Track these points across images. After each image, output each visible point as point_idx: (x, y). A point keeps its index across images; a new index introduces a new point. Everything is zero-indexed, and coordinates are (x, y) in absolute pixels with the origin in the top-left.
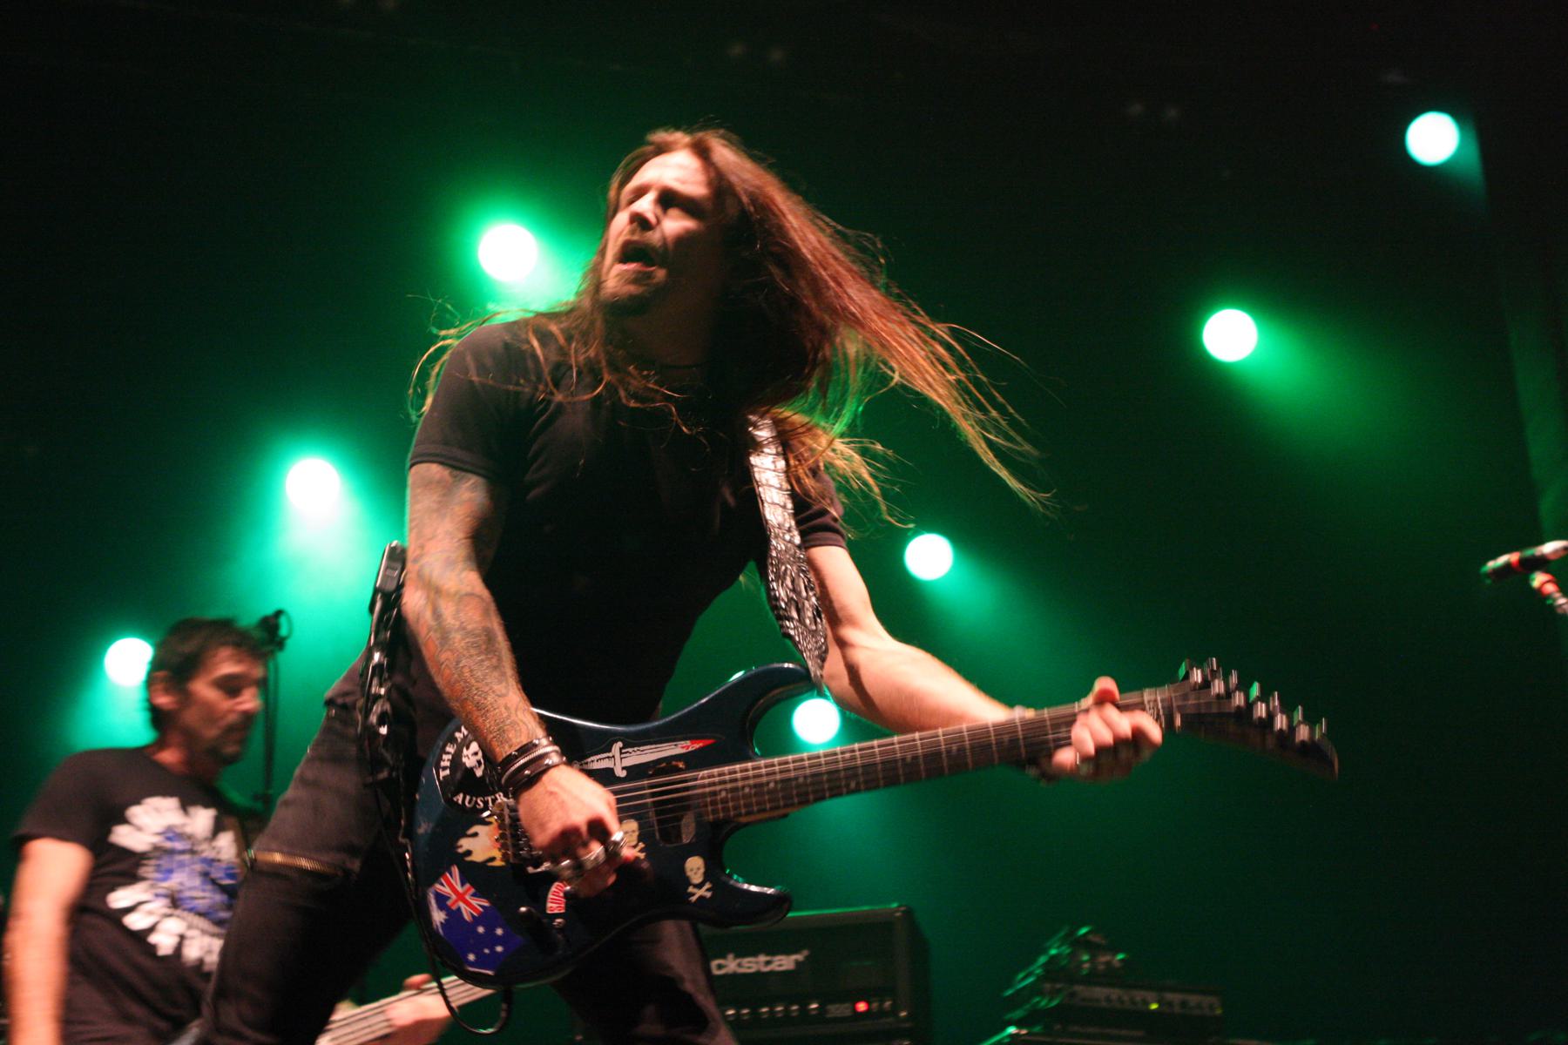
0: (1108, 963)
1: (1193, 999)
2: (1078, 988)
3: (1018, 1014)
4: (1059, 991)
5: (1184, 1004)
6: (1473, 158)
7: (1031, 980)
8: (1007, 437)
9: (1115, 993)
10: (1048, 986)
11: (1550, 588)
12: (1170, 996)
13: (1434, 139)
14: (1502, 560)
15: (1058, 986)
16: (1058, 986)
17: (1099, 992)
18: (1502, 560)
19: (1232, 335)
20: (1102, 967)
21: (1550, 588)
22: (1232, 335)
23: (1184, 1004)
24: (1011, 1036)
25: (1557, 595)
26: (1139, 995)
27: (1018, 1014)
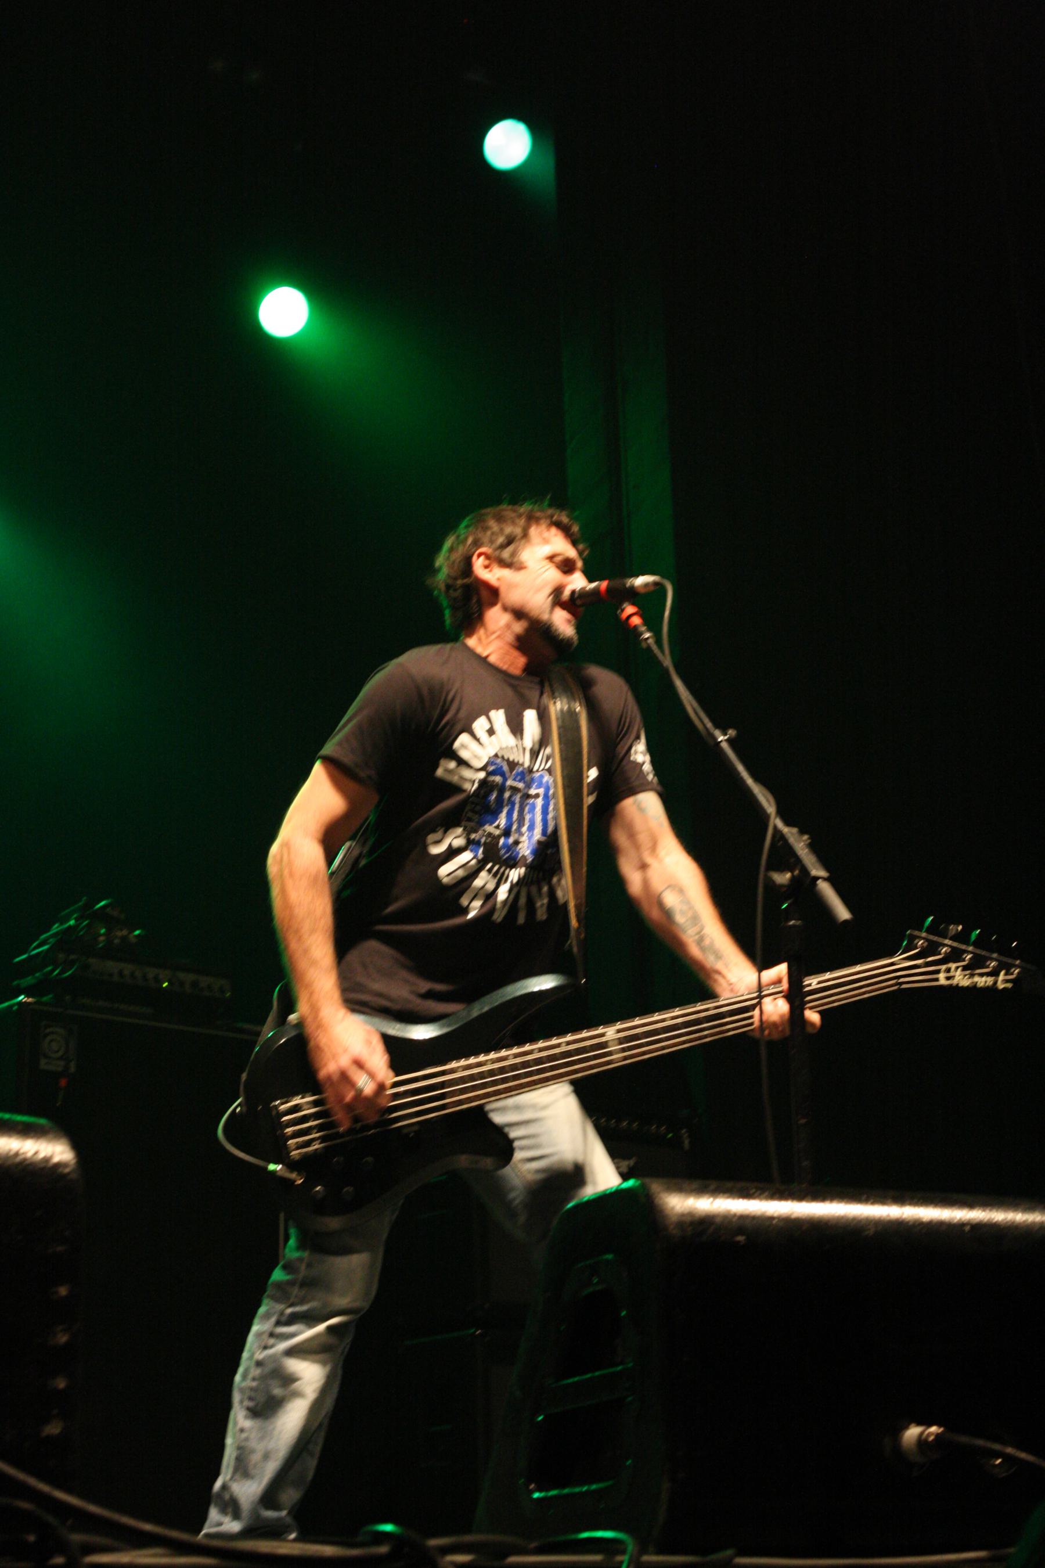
0: (124, 939)
1: (204, 981)
2: (92, 961)
3: (29, 981)
4: (72, 963)
5: (195, 984)
6: (548, 166)
7: (45, 947)
8: (659, 641)
9: (128, 968)
10: (61, 956)
11: (636, 620)
12: (182, 975)
13: (508, 145)
14: (102, 903)
15: (72, 957)
16: (72, 957)
17: (112, 966)
18: (102, 903)
19: (284, 312)
20: (117, 941)
21: (636, 620)
22: (284, 312)
23: (195, 984)
24: (20, 1003)
25: (643, 629)
26: (151, 972)
27: (29, 981)
